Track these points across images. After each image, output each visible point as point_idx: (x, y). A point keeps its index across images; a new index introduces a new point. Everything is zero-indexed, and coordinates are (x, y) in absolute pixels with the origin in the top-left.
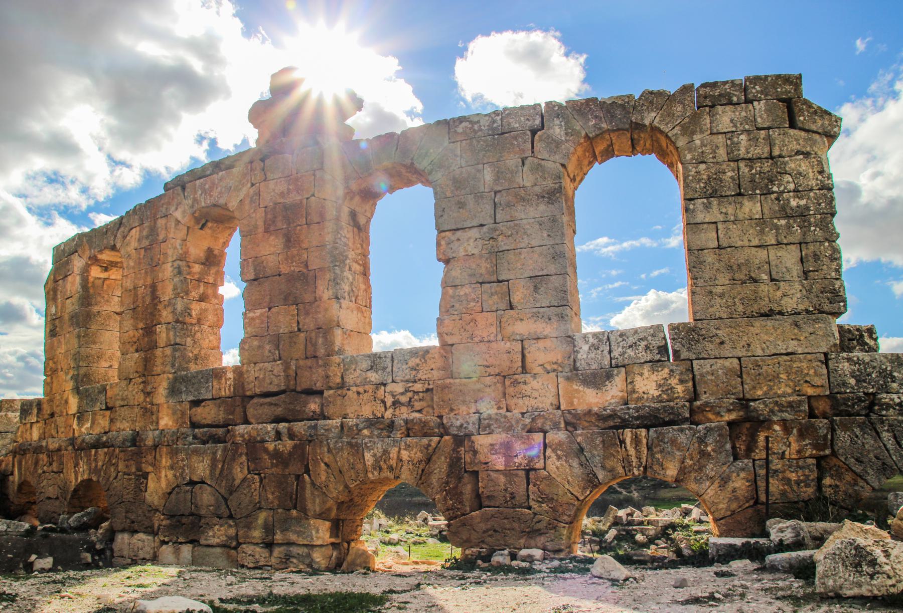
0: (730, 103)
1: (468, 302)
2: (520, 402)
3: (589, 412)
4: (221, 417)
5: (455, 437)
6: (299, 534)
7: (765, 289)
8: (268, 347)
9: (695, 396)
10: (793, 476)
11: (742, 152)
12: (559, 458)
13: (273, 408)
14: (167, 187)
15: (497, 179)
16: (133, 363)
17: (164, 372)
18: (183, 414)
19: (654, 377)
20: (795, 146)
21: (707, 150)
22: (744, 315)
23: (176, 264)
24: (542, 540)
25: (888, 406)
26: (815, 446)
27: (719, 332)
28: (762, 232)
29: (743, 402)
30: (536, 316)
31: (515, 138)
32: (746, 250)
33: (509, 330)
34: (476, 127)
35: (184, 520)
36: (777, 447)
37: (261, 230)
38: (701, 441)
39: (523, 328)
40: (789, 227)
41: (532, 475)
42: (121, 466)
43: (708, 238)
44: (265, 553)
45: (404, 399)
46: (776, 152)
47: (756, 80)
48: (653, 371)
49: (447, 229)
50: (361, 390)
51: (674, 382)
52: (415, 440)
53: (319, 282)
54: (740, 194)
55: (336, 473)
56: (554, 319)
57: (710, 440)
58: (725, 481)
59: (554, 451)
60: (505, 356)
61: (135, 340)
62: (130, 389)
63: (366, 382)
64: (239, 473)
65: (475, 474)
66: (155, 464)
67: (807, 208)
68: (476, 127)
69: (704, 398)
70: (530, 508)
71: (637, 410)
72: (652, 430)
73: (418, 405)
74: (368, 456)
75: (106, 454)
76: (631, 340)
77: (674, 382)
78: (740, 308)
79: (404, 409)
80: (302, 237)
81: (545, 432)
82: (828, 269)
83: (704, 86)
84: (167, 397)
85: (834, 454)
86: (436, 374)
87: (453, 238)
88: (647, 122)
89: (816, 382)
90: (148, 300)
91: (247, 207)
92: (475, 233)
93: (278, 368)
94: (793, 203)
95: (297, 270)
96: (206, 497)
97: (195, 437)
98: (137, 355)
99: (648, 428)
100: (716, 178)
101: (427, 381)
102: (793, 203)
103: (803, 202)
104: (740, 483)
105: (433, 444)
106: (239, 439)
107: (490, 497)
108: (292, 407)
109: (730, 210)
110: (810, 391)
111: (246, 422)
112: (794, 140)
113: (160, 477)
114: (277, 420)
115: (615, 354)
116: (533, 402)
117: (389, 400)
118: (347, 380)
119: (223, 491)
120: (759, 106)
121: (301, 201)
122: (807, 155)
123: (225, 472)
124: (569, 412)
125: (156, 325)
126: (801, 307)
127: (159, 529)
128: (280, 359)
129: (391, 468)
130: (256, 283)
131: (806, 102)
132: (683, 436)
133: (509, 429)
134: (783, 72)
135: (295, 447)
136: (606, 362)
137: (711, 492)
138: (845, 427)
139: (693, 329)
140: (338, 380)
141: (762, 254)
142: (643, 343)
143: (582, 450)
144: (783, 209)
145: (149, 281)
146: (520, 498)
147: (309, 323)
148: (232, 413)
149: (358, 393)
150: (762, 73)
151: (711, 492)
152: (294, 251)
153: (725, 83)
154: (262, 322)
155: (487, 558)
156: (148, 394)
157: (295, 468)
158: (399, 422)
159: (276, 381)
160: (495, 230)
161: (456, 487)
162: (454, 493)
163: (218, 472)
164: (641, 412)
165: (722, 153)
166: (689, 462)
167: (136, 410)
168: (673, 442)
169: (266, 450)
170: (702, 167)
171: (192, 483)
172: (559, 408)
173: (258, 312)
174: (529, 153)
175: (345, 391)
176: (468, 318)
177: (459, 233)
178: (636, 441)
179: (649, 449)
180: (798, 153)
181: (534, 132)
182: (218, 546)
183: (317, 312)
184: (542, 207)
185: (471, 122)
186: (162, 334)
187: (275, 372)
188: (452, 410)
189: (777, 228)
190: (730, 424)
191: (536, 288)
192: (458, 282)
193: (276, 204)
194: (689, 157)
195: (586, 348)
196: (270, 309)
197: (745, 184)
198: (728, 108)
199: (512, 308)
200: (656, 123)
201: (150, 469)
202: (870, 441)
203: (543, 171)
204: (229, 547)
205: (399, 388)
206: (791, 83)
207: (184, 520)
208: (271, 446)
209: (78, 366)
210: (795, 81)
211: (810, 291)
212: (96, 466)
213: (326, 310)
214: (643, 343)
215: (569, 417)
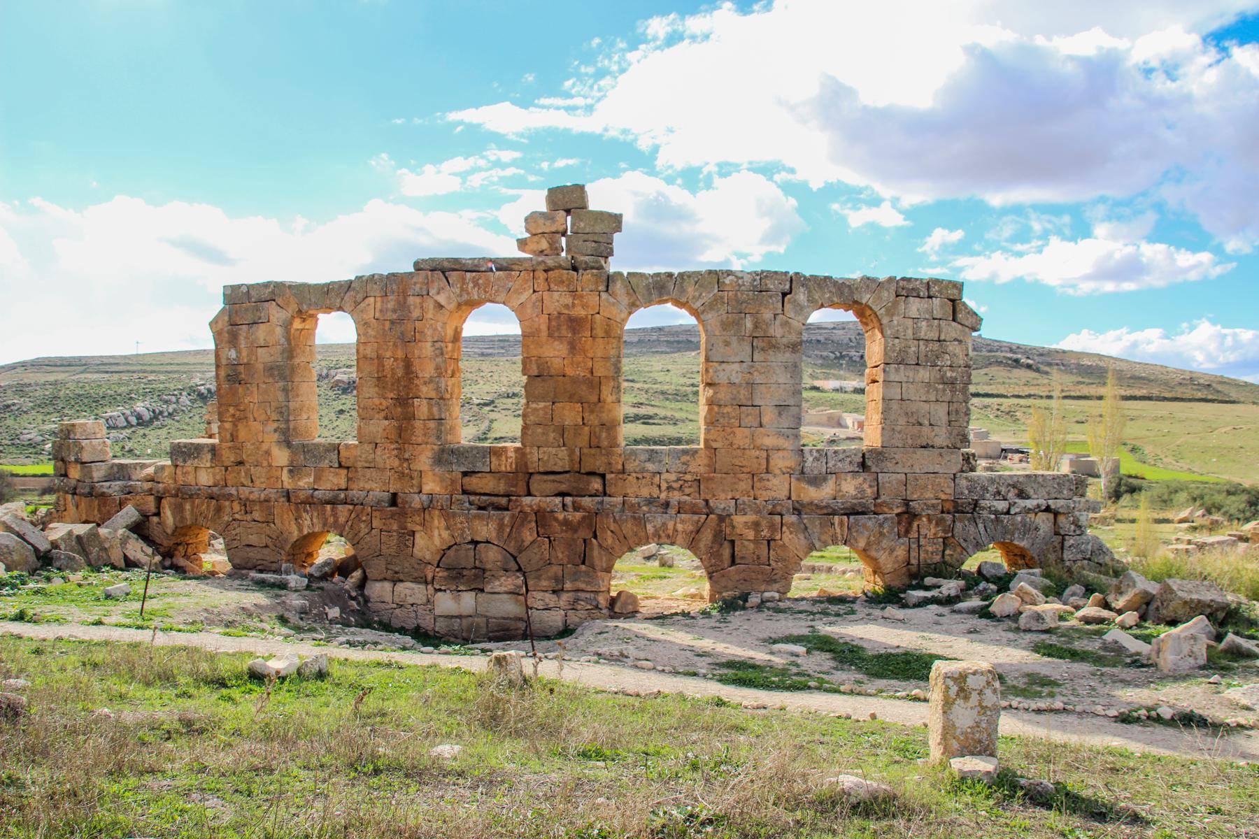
4: (494, 488)
5: (719, 516)
6: (588, 583)
7: (926, 430)
8: (552, 435)
9: (878, 496)
10: (930, 549)
11: (922, 335)
15: (756, 327)
16: (380, 430)
18: (453, 482)
19: (853, 482)
20: (954, 335)
22: (912, 446)
24: (776, 586)
25: (984, 508)
26: (945, 531)
28: (928, 392)
29: (906, 502)
30: (779, 434)
33: (759, 442)
35: (465, 572)
36: (923, 531)
37: (545, 333)
38: (881, 525)
39: (769, 442)
40: (944, 390)
43: (895, 393)
44: (554, 597)
48: (853, 478)
51: (865, 486)
53: (603, 388)
57: (886, 525)
58: (892, 550)
63: (643, 470)
64: (528, 535)
65: (733, 542)
67: (956, 379)
69: (883, 498)
72: (852, 518)
74: (650, 527)
76: (841, 456)
77: (865, 486)
78: (910, 442)
79: (676, 493)
81: (782, 515)
83: (903, 279)
85: (953, 536)
86: (702, 469)
88: (864, 302)
89: (948, 492)
90: (400, 373)
93: (563, 453)
94: (949, 374)
96: (492, 556)
97: (471, 503)
98: (387, 422)
99: (848, 515)
101: (696, 474)
102: (949, 374)
104: (901, 552)
106: (528, 510)
109: (911, 374)
110: (943, 497)
111: (529, 494)
114: (562, 494)
115: (830, 465)
117: (664, 486)
118: (627, 467)
119: (511, 551)
120: (936, 301)
122: (960, 342)
129: (668, 536)
131: (964, 304)
132: (869, 522)
133: (758, 512)
135: (584, 517)
138: (961, 521)
139: (880, 453)
140: (620, 467)
141: (926, 406)
143: (806, 528)
144: (942, 377)
147: (593, 419)
148: (515, 486)
154: (546, 413)
155: (745, 597)
158: (674, 502)
159: (561, 463)
163: (506, 535)
165: (910, 332)
168: (864, 526)
169: (556, 519)
170: (897, 341)
171: (475, 543)
172: (789, 498)
173: (542, 405)
174: (780, 311)
178: (841, 523)
180: (955, 340)
181: (784, 295)
182: (506, 593)
184: (788, 355)
189: (937, 390)
190: (898, 515)
201: (418, 528)
205: (673, 477)
207: (465, 572)
208: (561, 516)
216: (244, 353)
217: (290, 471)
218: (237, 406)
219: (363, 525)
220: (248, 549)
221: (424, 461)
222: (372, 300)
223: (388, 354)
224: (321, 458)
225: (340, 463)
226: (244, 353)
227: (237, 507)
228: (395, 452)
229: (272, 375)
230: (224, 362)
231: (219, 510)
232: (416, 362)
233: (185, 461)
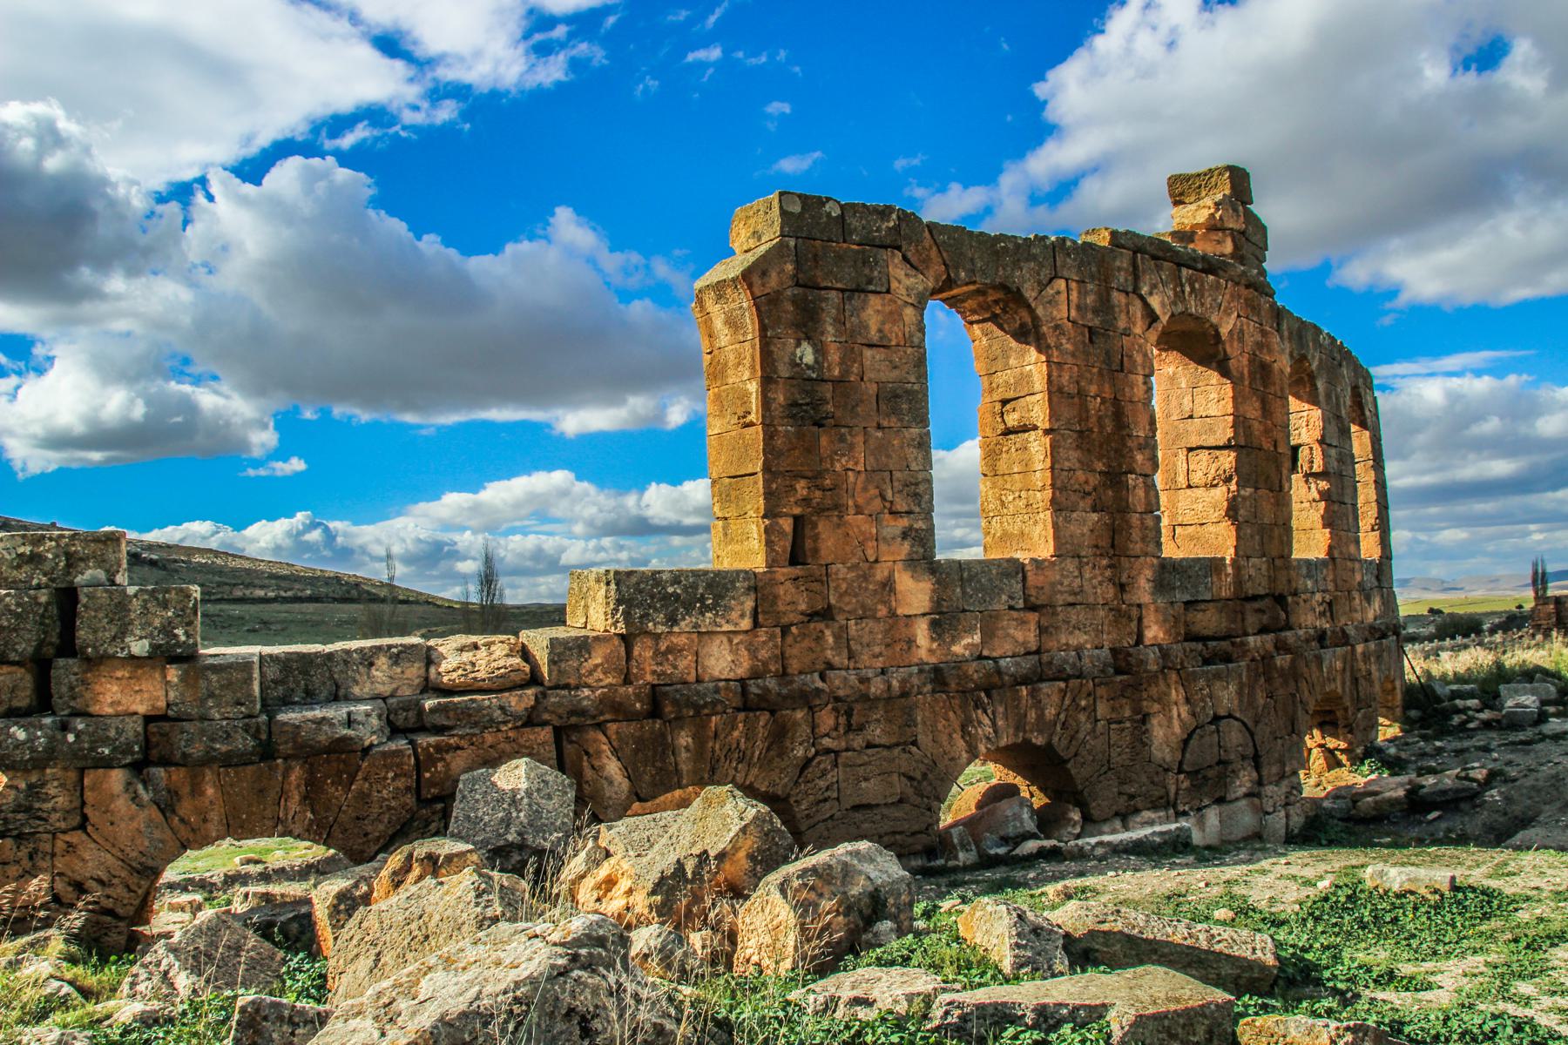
17: (1146, 555)
42: (1102, 709)
61: (1088, 488)
62: (1087, 576)
66: (1162, 700)
75: (1063, 693)
84: (1153, 594)
98: (1095, 516)
125: (1126, 473)
127: (1177, 793)
156: (1122, 588)
167: (1102, 613)
171: (1217, 719)
193: (971, 323)
212: (1041, 716)
216: (834, 356)
217: (934, 625)
218: (815, 478)
219: (1082, 717)
220: (858, 816)
221: (1143, 591)
222: (1061, 284)
223: (1093, 389)
224: (992, 592)
225: (1026, 598)
226: (834, 356)
227: (826, 719)
228: (1108, 573)
229: (895, 411)
230: (784, 371)
231: (780, 735)
232: (1128, 408)
233: (672, 620)
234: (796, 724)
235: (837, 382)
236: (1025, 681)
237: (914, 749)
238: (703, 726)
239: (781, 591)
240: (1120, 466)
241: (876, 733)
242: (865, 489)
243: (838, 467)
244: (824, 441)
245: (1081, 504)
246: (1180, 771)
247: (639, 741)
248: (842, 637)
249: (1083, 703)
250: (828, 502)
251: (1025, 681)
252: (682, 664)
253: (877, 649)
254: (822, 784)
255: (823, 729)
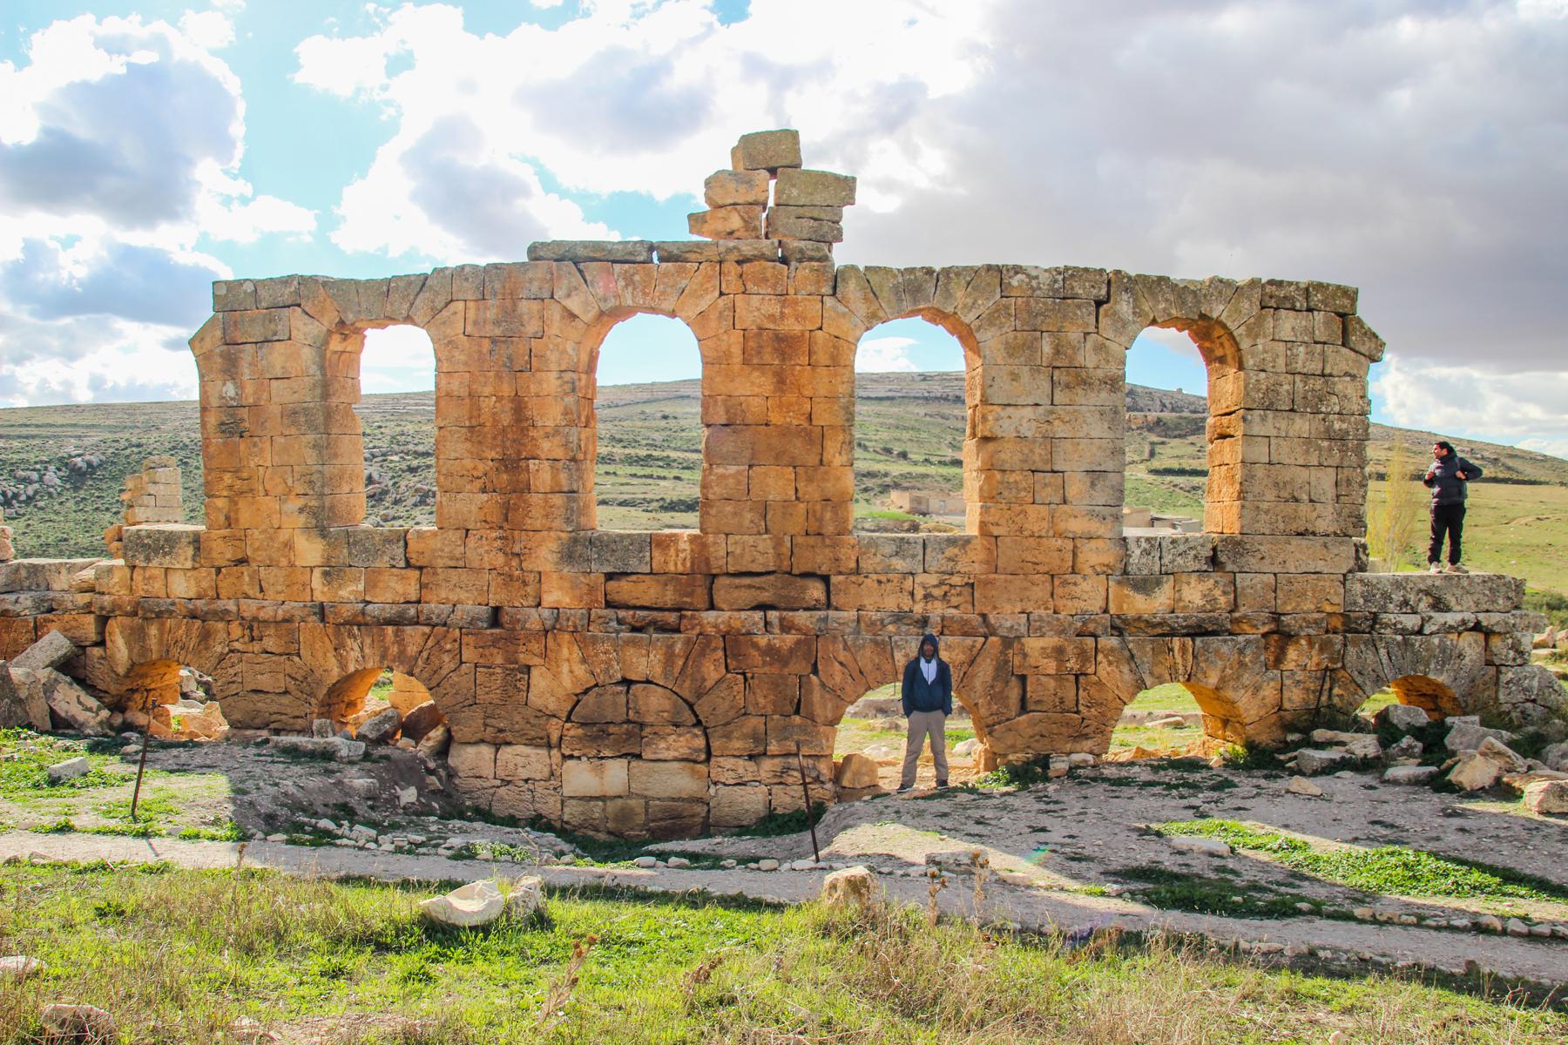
0: (1293, 309)
1: (1019, 491)
2: (1069, 603)
3: (1139, 619)
5: (1004, 638)
7: (1304, 508)
8: (749, 516)
11: (1299, 367)
12: (1110, 663)
13: (754, 592)
14: (535, 252)
15: (1057, 352)
18: (591, 589)
19: (1200, 587)
21: (1268, 357)
22: (1284, 533)
23: (568, 376)
25: (1387, 626)
27: (1262, 548)
28: (1307, 452)
29: (1276, 617)
31: (1079, 307)
32: (1293, 469)
33: (1062, 526)
34: (1034, 283)
35: (612, 729)
37: (737, 358)
38: (1241, 652)
39: (1076, 526)
40: (1330, 449)
41: (1082, 679)
45: (937, 592)
46: (1327, 371)
47: (1320, 287)
49: (944, 378)
50: (883, 578)
51: (1217, 593)
52: (957, 639)
53: (828, 443)
54: (1292, 410)
55: (856, 674)
56: (1109, 519)
57: (1248, 652)
58: (1257, 689)
59: (1106, 656)
60: (1056, 554)
63: (888, 570)
64: (712, 671)
65: (1023, 679)
68: (1034, 283)
69: (1243, 610)
70: (1077, 712)
71: (1185, 619)
73: (955, 600)
74: (898, 656)
76: (1182, 548)
77: (1217, 593)
78: (1282, 526)
79: (938, 604)
80: (803, 381)
81: (1095, 636)
82: (1356, 496)
83: (1271, 282)
85: (1343, 667)
86: (977, 568)
87: (1003, 414)
89: (1335, 600)
90: (506, 419)
91: (713, 324)
92: (1028, 412)
93: (765, 543)
94: (1337, 426)
95: (795, 422)
98: (485, 497)
100: (1272, 390)
101: (968, 574)
102: (1337, 426)
103: (1344, 426)
105: (978, 646)
106: (710, 630)
107: (1038, 702)
108: (783, 592)
110: (1329, 609)
112: (1340, 360)
113: (560, 673)
114: (763, 607)
115: (1165, 561)
116: (1082, 604)
117: (919, 593)
119: (686, 695)
121: (803, 332)
122: (1353, 377)
123: (689, 670)
124: (1119, 617)
126: (1331, 529)
128: (767, 531)
130: (728, 430)
131: (1359, 321)
134: (1343, 283)
136: (1156, 569)
137: (1244, 700)
138: (1355, 644)
140: (853, 565)
141: (1304, 474)
142: (1193, 552)
143: (1132, 657)
144: (1327, 430)
145: (507, 390)
146: (1070, 703)
148: (691, 595)
149: (880, 582)
150: (1325, 281)
151: (1244, 700)
152: (791, 397)
153: (1290, 284)
154: (739, 482)
157: (799, 667)
159: (761, 559)
160: (1052, 412)
161: (1002, 692)
162: (997, 697)
164: (1189, 622)
165: (1281, 361)
166: (1229, 671)
168: (1217, 651)
169: (755, 646)
170: (1263, 375)
174: (1092, 329)
175: (861, 579)
176: (1018, 508)
177: (1010, 410)
178: (1183, 649)
179: (1194, 657)
180: (1347, 374)
181: (1099, 304)
183: (823, 480)
185: (1028, 275)
186: (541, 475)
187: (760, 548)
188: (995, 608)
189: (1320, 449)
190: (1264, 635)
191: (1093, 485)
192: (1007, 467)
194: (1251, 362)
195: (1138, 552)
196: (750, 466)
197: (1298, 400)
198: (1292, 313)
199: (1065, 502)
200: (1223, 318)
202: (1370, 656)
203: (1107, 353)
204: (695, 762)
205: (932, 580)
206: (1349, 297)
207: (612, 729)
208: (762, 641)
209: (322, 495)
210: (1351, 295)
211: (1339, 515)
212: (402, 652)
213: (838, 479)
214: (1193, 552)
215: (1118, 622)
216: (249, 389)
217: (326, 574)
219: (446, 658)
220: (255, 697)
231: (206, 636)
232: (532, 403)
233: (148, 559)
234: (217, 631)
235: (255, 406)
236: (388, 622)
237: (296, 659)
238: (163, 625)
239: (214, 545)
240: (519, 453)
241: (270, 643)
242: (271, 479)
243: (252, 464)
244: (242, 447)
245: (468, 487)
246: (568, 720)
247: (132, 628)
248: (255, 576)
249: (448, 647)
250: (245, 488)
251: (388, 622)
252: (157, 586)
253: (279, 588)
254: (232, 671)
255: (234, 637)
